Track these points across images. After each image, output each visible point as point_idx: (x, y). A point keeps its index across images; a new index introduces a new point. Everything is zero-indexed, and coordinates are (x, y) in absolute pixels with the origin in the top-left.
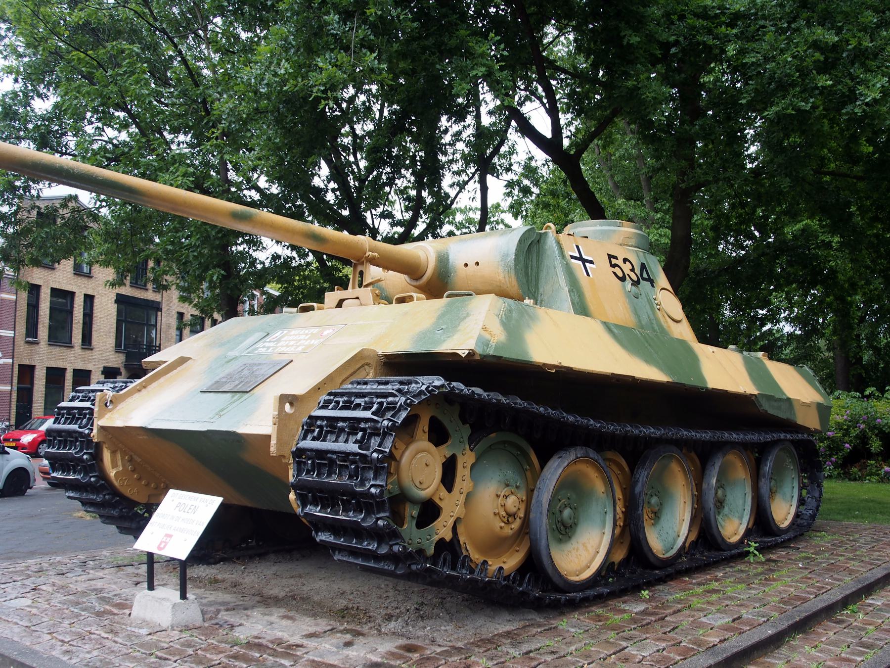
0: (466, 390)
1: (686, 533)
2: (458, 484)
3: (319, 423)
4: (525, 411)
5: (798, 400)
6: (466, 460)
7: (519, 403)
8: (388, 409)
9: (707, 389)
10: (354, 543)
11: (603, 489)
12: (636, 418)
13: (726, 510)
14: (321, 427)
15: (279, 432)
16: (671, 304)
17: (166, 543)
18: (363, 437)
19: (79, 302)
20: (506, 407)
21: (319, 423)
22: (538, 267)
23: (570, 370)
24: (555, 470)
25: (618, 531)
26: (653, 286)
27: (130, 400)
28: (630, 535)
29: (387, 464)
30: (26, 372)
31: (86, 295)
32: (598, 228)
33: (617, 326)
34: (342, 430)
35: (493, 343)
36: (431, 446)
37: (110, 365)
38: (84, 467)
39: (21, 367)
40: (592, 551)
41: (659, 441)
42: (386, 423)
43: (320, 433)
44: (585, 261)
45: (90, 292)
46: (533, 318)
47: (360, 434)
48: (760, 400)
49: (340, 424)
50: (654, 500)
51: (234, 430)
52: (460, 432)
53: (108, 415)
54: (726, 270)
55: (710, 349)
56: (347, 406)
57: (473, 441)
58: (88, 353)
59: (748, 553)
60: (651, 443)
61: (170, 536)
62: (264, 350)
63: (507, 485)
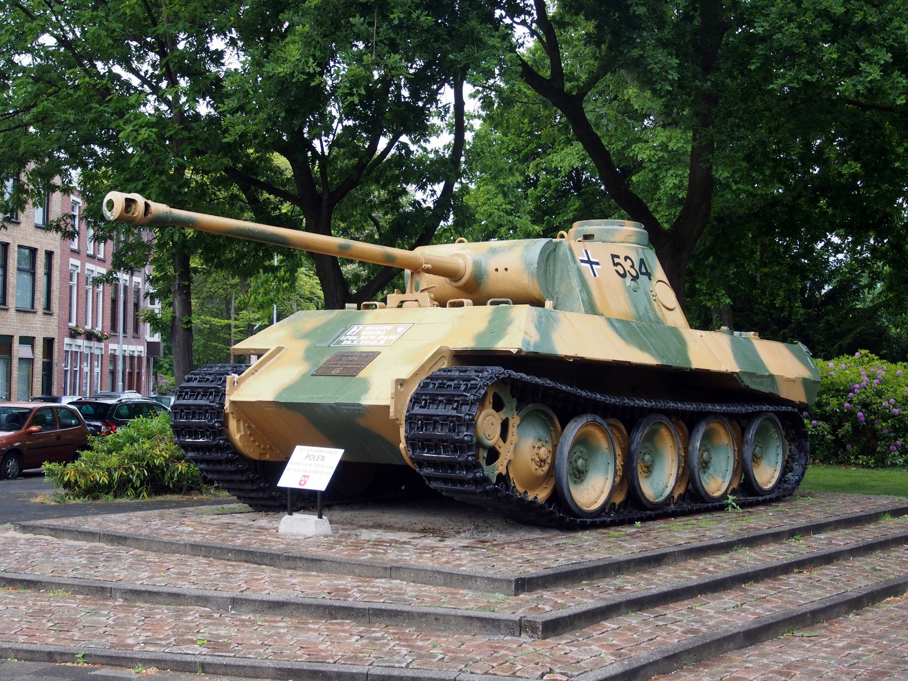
1: (673, 484)
2: (510, 437)
4: (553, 388)
5: (782, 377)
6: (514, 421)
7: (549, 383)
11: (606, 446)
12: (634, 393)
13: (711, 470)
14: (426, 400)
15: (395, 403)
16: (665, 294)
18: (457, 406)
20: (549, 387)
22: (554, 270)
23: (583, 359)
24: (573, 429)
25: (618, 479)
26: (650, 279)
27: (248, 381)
28: (627, 481)
29: (471, 424)
32: (604, 227)
33: (617, 320)
34: (441, 401)
35: (532, 343)
36: (494, 412)
40: (598, 491)
41: (651, 411)
43: (425, 404)
44: (591, 263)
46: (556, 320)
48: (741, 376)
50: (647, 457)
52: (511, 403)
53: (236, 392)
54: (756, 215)
57: (518, 409)
59: (728, 505)
60: (645, 412)
62: (349, 342)
63: (540, 440)
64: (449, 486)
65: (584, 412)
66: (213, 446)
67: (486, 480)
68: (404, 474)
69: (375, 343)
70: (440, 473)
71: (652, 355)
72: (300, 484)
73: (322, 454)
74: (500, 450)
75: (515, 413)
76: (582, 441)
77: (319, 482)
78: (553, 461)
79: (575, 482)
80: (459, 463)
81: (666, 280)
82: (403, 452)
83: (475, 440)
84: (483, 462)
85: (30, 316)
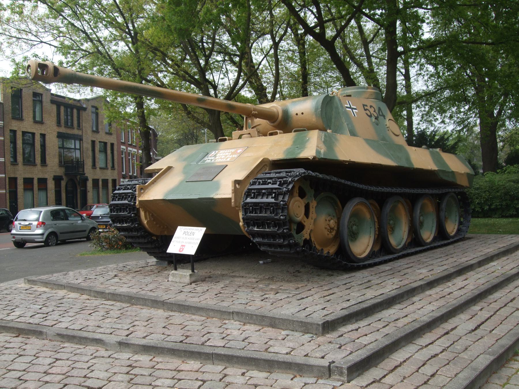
0: (313, 174)
3: (253, 191)
6: (313, 204)
7: (335, 179)
8: (284, 183)
9: (414, 168)
10: (272, 241)
14: (254, 193)
17: (183, 249)
18: (275, 196)
19: (38, 138)
21: (253, 191)
23: (354, 162)
24: (351, 207)
26: (385, 119)
27: (150, 188)
29: (285, 207)
30: (13, 181)
31: (41, 134)
34: (264, 194)
37: (57, 174)
38: (131, 220)
39: (10, 178)
42: (285, 189)
43: (254, 195)
44: (352, 109)
45: (43, 132)
46: (336, 140)
47: (274, 195)
49: (264, 191)
50: (391, 222)
51: (211, 196)
52: (310, 193)
55: (414, 148)
56: (265, 183)
57: (315, 197)
58: (45, 168)
61: (184, 246)
62: (209, 161)
63: (329, 215)
64: (273, 249)
65: (355, 196)
66: (132, 228)
67: (296, 245)
68: (245, 239)
69: (225, 160)
70: (266, 241)
71: (392, 160)
72: (180, 251)
73: (193, 231)
74: (305, 224)
75: (313, 199)
76: (355, 215)
77: (191, 250)
78: (338, 228)
79: (352, 241)
80: (278, 234)
81: (392, 119)
82: (242, 228)
83: (288, 218)
84: (294, 232)
85: (105, 171)
